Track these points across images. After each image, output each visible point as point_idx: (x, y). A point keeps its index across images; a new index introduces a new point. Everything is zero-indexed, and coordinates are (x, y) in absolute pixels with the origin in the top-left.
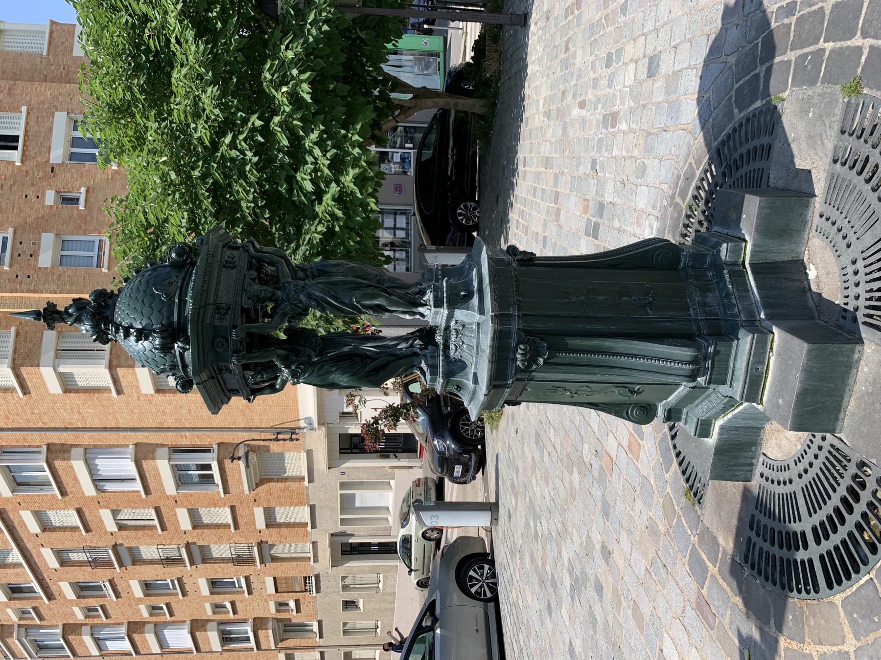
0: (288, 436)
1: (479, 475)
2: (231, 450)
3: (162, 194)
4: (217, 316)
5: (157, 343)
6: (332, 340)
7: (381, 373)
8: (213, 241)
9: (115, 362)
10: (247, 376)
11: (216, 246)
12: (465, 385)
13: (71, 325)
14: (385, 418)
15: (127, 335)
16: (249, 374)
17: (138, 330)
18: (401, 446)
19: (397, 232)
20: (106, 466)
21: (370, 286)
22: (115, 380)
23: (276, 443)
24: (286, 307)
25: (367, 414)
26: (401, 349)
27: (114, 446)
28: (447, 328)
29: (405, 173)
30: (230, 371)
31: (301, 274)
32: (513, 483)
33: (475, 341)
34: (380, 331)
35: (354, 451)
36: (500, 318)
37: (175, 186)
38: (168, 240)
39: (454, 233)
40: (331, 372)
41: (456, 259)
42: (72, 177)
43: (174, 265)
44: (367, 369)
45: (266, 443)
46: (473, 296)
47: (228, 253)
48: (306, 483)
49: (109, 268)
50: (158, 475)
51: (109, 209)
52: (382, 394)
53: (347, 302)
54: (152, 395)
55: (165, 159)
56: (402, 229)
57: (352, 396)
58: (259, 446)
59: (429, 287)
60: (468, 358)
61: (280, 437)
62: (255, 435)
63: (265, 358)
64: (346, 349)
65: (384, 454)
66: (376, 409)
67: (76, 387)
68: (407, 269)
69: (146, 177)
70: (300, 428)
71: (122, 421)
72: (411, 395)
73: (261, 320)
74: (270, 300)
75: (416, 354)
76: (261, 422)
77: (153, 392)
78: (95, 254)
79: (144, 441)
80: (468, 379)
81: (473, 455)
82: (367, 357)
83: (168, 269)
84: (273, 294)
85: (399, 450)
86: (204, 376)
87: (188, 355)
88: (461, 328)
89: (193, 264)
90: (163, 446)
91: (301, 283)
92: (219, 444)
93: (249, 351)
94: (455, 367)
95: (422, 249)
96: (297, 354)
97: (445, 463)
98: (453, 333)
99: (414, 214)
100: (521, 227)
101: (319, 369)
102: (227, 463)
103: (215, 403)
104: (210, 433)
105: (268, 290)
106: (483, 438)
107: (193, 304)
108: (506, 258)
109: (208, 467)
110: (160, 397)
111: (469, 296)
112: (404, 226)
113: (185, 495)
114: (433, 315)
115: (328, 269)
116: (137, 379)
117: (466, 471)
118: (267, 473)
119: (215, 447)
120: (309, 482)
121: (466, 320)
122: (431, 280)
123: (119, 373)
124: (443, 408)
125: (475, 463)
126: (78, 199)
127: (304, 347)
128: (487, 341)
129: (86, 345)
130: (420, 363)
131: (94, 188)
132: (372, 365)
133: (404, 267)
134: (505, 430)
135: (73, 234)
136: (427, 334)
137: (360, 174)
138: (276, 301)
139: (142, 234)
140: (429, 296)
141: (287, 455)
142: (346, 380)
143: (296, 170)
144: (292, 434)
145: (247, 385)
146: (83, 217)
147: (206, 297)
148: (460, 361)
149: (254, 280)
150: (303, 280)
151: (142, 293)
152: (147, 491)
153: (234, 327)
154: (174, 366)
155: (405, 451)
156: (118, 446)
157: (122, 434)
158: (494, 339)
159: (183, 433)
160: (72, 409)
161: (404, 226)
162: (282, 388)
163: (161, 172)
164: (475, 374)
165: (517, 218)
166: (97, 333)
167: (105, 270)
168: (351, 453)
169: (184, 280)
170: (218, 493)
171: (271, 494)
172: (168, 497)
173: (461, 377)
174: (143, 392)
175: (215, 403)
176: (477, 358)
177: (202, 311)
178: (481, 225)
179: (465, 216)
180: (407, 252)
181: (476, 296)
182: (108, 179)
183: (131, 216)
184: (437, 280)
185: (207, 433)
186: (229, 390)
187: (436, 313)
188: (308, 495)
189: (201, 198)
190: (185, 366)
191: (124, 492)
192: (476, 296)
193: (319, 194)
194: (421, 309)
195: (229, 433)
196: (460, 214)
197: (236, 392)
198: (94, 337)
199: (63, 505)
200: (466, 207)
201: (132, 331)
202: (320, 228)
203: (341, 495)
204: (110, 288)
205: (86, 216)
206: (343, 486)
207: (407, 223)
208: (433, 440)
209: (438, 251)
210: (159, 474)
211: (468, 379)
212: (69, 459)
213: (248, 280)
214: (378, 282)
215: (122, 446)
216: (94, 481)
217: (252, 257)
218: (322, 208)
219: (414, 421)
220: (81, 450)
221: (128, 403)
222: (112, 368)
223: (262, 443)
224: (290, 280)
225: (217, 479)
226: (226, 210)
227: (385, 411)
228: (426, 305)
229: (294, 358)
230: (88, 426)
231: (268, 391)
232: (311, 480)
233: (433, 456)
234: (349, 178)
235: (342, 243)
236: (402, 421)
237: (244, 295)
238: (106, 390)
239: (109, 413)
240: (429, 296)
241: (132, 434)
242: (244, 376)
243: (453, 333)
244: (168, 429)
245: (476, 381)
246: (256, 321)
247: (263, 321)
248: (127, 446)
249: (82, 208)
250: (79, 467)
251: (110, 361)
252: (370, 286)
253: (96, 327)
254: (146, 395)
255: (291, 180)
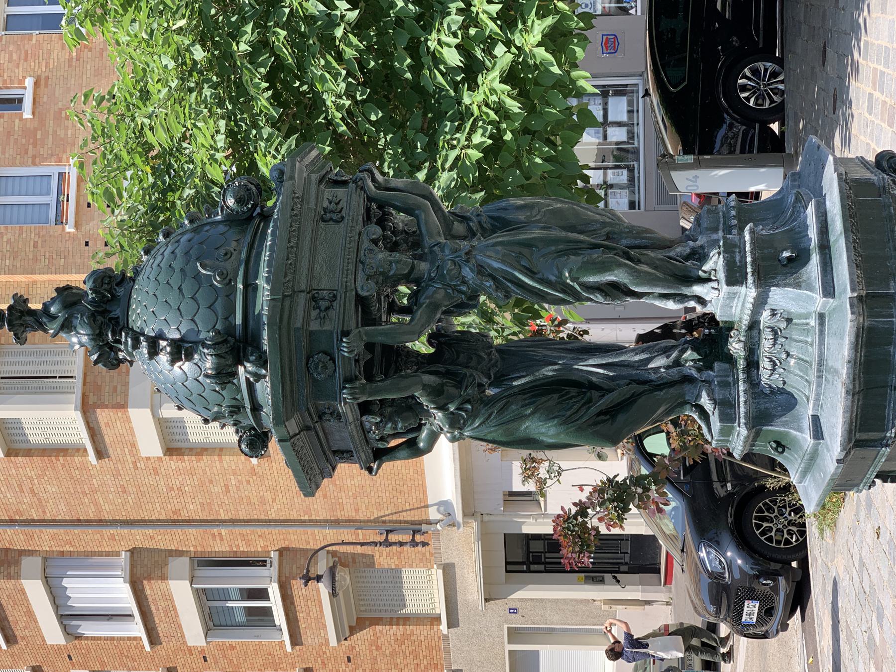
0: (406, 537)
1: (795, 621)
2: (303, 562)
3: (179, 89)
4: (314, 313)
5: (208, 365)
6: (514, 357)
7: (621, 418)
8: (301, 170)
9: (92, 399)
10: (367, 425)
11: (308, 180)
12: (795, 441)
13: (55, 335)
14: (600, 505)
15: (154, 351)
16: (371, 420)
17: (174, 343)
18: (627, 558)
19: (611, 131)
20: (82, 591)
21: (596, 246)
22: (94, 432)
23: (385, 550)
24: (437, 292)
25: (562, 497)
26: (656, 369)
27: (94, 554)
28: (754, 325)
29: (625, 11)
30: (339, 417)
31: (459, 228)
32: (871, 639)
33: (814, 351)
34: (586, 332)
35: (534, 567)
36: (869, 302)
37: (200, 72)
38: (192, 173)
39: (731, 126)
40: (522, 418)
41: (766, 182)
42: (10, 60)
43: (232, 220)
44: (593, 410)
45: (367, 550)
46: (807, 259)
47: (328, 193)
48: (444, 627)
49: (77, 225)
50: (171, 610)
51: (80, 115)
52: (593, 456)
53: (553, 278)
54: (159, 459)
55: (182, 23)
56: (620, 124)
57: (533, 460)
58: (354, 555)
59: (714, 244)
60: (797, 385)
61: (393, 538)
62: (347, 535)
63: (400, 390)
64: (548, 371)
65: (595, 574)
66: (581, 488)
67: (24, 446)
68: (632, 205)
69: (149, 59)
70: (429, 523)
71: (106, 507)
72: (649, 458)
73: (384, 318)
74: (407, 279)
75: (688, 379)
76: (357, 510)
77: (161, 455)
78: (51, 199)
79: (146, 545)
80: (800, 429)
81: (782, 581)
82: (592, 386)
83: (222, 228)
84: (413, 268)
85: (624, 568)
86: (293, 426)
87: (264, 389)
88: (783, 325)
89: (266, 217)
90: (180, 553)
91: (464, 245)
92: (281, 552)
93: (370, 378)
94: (771, 406)
95: (666, 162)
96: (459, 382)
97: (724, 595)
98: (767, 335)
99: (647, 94)
100: (878, 109)
101: (501, 411)
102: (297, 585)
103: (311, 472)
104: (265, 530)
105: (403, 259)
106: (803, 546)
107: (272, 292)
108: (874, 177)
109: (262, 594)
110: (173, 463)
111: (800, 259)
112: (624, 118)
113: (221, 648)
114: (724, 300)
115: (510, 216)
116: (131, 428)
117: (767, 612)
118: (370, 609)
119: (274, 555)
120: (449, 626)
121: (794, 308)
122: (716, 230)
123: (100, 419)
124: (717, 485)
125: (787, 596)
126: (20, 101)
127: (467, 367)
128: (841, 351)
129: (42, 368)
130: (699, 396)
131: (47, 78)
132: (604, 402)
133: (625, 202)
134: (852, 531)
135: (14, 165)
136: (710, 336)
137: (554, 28)
138: (417, 282)
139: (138, 160)
140: (715, 263)
141: (407, 574)
142: (552, 431)
143: (427, 28)
144: (415, 532)
145: (367, 442)
146: (29, 133)
147: (294, 278)
148: (782, 391)
149: (375, 242)
150: (464, 238)
151: (177, 274)
152: (153, 637)
153: (346, 334)
154: (238, 408)
155: (634, 569)
156: (100, 554)
157: (109, 531)
158: (856, 346)
159: (215, 530)
160: (20, 486)
161: (624, 118)
162: (429, 449)
163: (174, 47)
164: (816, 420)
165: (869, 90)
166: (100, 348)
167: (70, 229)
168: (529, 571)
169: (251, 247)
170: (282, 644)
171: (378, 648)
172: (190, 650)
173: (785, 424)
174: (144, 454)
175: (311, 472)
176: (819, 385)
177: (287, 303)
178: (789, 107)
179: (754, 91)
180: (631, 170)
181: (815, 259)
182: (70, 60)
183: (118, 129)
184: (728, 229)
185: (259, 530)
186: (335, 452)
187: (731, 297)
188: (447, 651)
189: (252, 91)
190: (256, 408)
191: (112, 639)
192: (815, 259)
193: (471, 71)
194: (698, 290)
195: (300, 530)
196: (744, 88)
197: (345, 455)
198: (95, 357)
199: (9, 661)
200: (756, 72)
201: (163, 343)
202: (477, 139)
203: (510, 652)
204: (114, 263)
205: (36, 130)
206: (515, 634)
207: (630, 112)
208: (698, 550)
209: (698, 165)
210: (174, 606)
211: (800, 429)
212: (18, 577)
213: (366, 244)
214: (608, 237)
215: (108, 554)
216: (61, 618)
217: (370, 199)
218: (479, 97)
219: (660, 511)
220: (38, 561)
221: (116, 475)
222: (87, 409)
223: (359, 549)
224: (442, 240)
225: (279, 617)
226: (300, 113)
227: (599, 491)
228: (708, 280)
229: (452, 390)
230: (48, 517)
231: (403, 453)
232: (453, 623)
233: (697, 581)
234: (536, 36)
235: (518, 164)
236: (634, 510)
237: (360, 272)
238: (78, 450)
239: (84, 493)
240: (715, 263)
241: (125, 531)
242: (362, 424)
243: (767, 335)
244: (189, 522)
245: (818, 433)
246: (375, 322)
247: (388, 321)
248: (117, 554)
249: (27, 114)
250: (35, 590)
251: (84, 397)
252: (596, 246)
253: (98, 336)
254: (148, 459)
255: (415, 48)
